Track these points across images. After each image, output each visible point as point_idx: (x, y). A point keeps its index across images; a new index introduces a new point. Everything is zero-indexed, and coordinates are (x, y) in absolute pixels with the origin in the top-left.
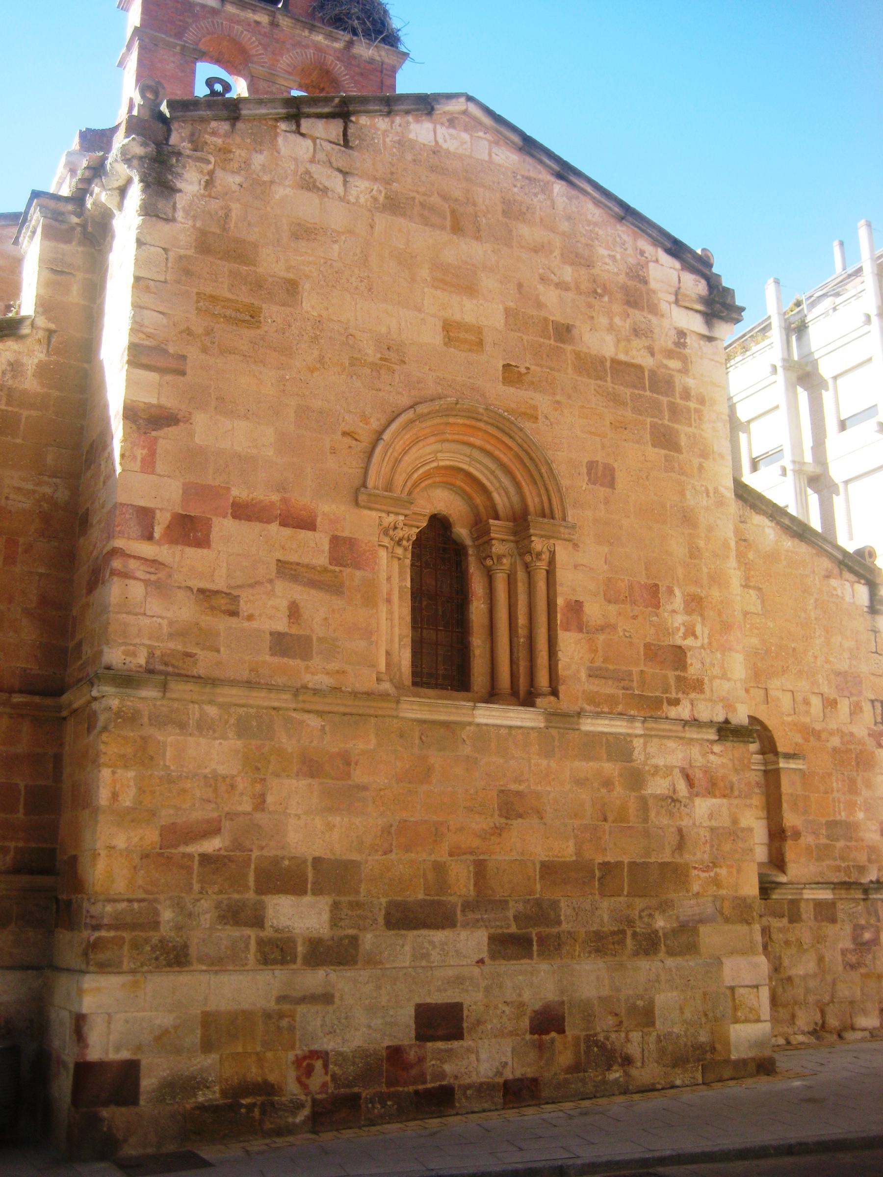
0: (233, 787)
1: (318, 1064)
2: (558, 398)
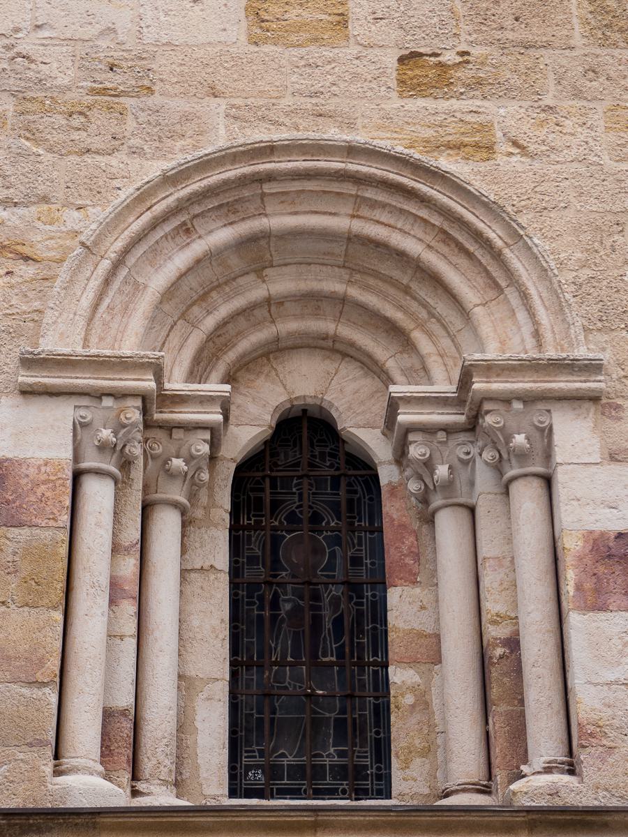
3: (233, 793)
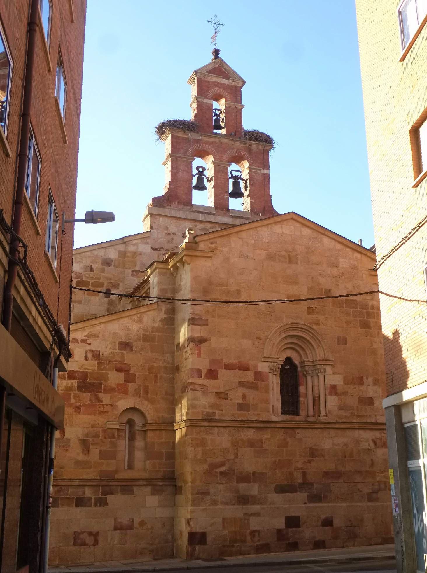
0: (228, 451)
1: (256, 534)
2: (327, 316)
3: (100, 459)
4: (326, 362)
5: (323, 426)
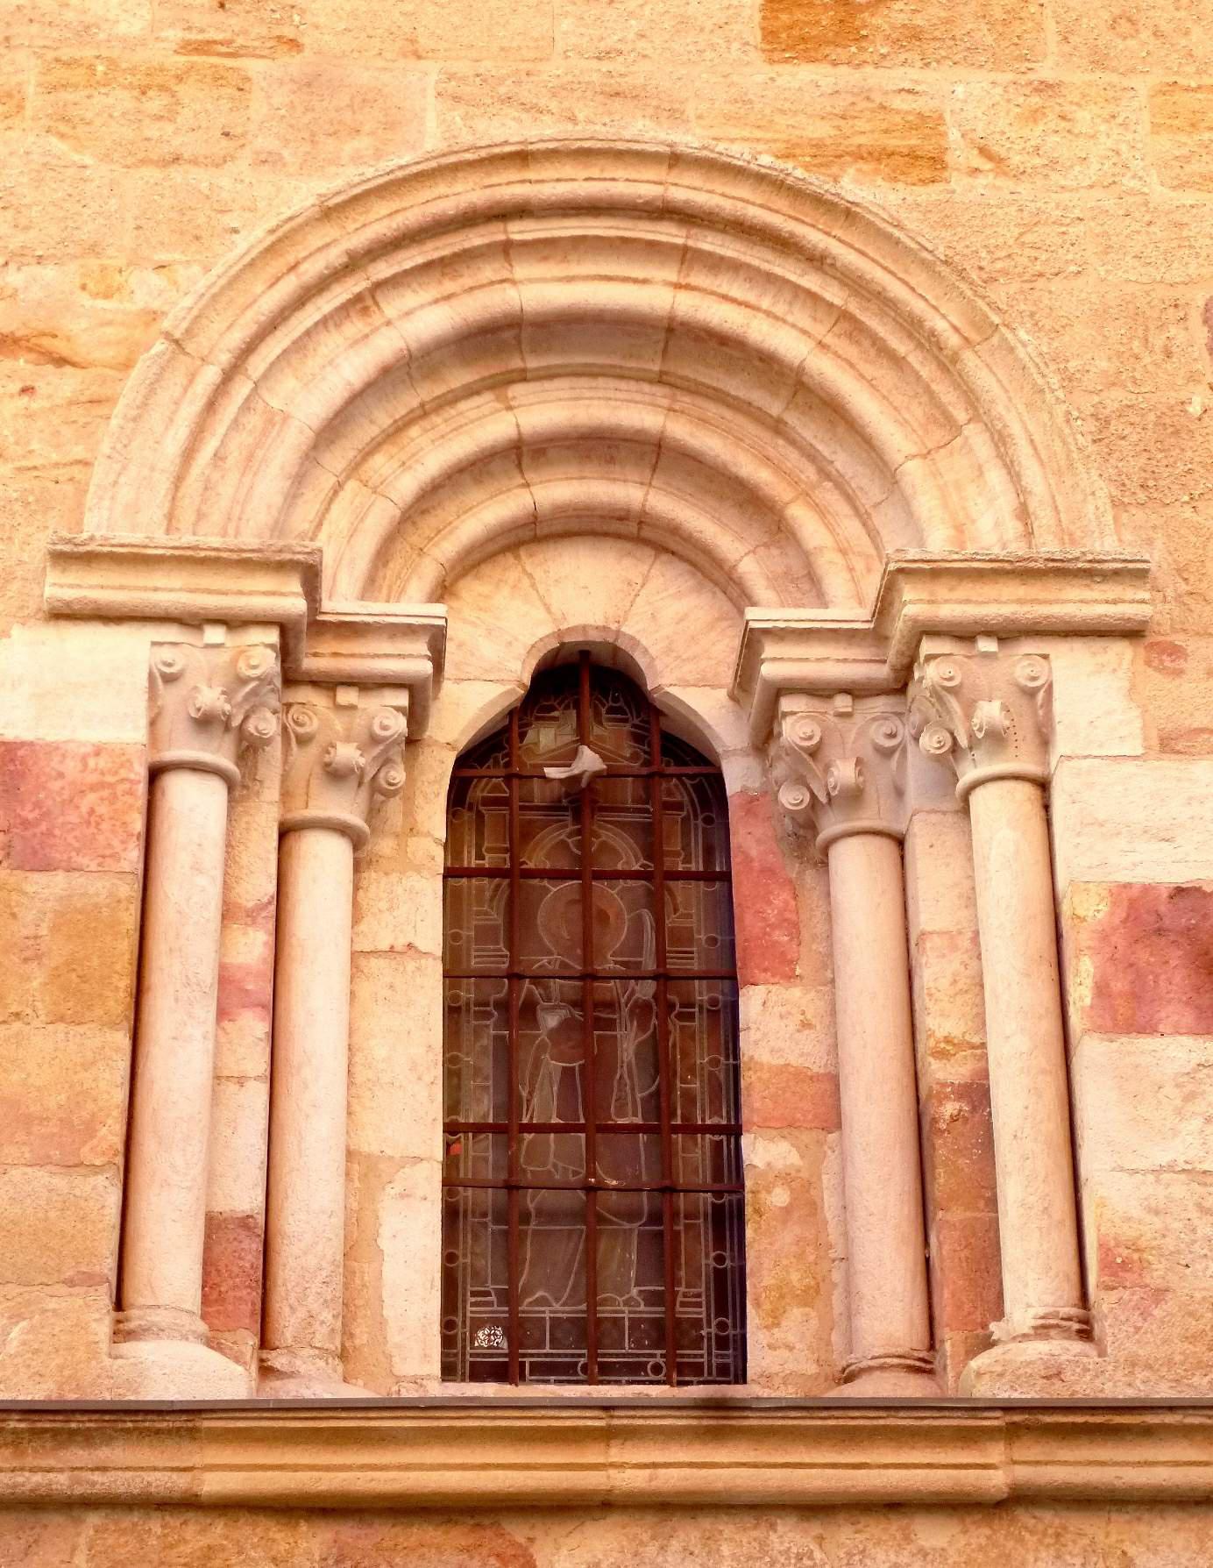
4: (1059, 601)
5: (994, 1469)
